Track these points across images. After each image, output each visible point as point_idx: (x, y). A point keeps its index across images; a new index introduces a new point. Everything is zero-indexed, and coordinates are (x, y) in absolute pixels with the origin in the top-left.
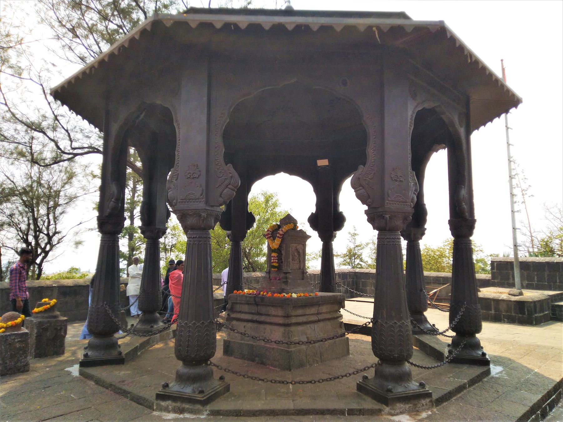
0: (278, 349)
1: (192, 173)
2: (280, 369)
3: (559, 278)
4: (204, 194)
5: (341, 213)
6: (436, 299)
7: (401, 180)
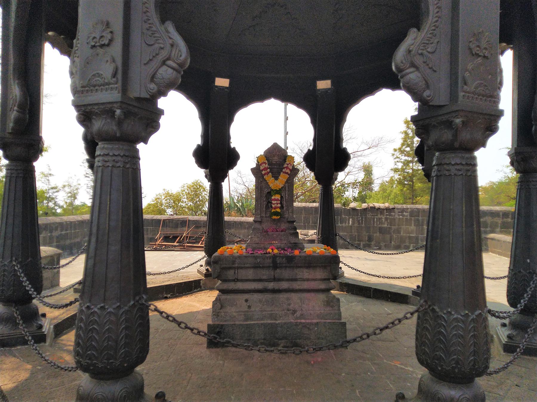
0: (325, 323)
1: (98, 37)
4: (120, 76)
7: (486, 55)
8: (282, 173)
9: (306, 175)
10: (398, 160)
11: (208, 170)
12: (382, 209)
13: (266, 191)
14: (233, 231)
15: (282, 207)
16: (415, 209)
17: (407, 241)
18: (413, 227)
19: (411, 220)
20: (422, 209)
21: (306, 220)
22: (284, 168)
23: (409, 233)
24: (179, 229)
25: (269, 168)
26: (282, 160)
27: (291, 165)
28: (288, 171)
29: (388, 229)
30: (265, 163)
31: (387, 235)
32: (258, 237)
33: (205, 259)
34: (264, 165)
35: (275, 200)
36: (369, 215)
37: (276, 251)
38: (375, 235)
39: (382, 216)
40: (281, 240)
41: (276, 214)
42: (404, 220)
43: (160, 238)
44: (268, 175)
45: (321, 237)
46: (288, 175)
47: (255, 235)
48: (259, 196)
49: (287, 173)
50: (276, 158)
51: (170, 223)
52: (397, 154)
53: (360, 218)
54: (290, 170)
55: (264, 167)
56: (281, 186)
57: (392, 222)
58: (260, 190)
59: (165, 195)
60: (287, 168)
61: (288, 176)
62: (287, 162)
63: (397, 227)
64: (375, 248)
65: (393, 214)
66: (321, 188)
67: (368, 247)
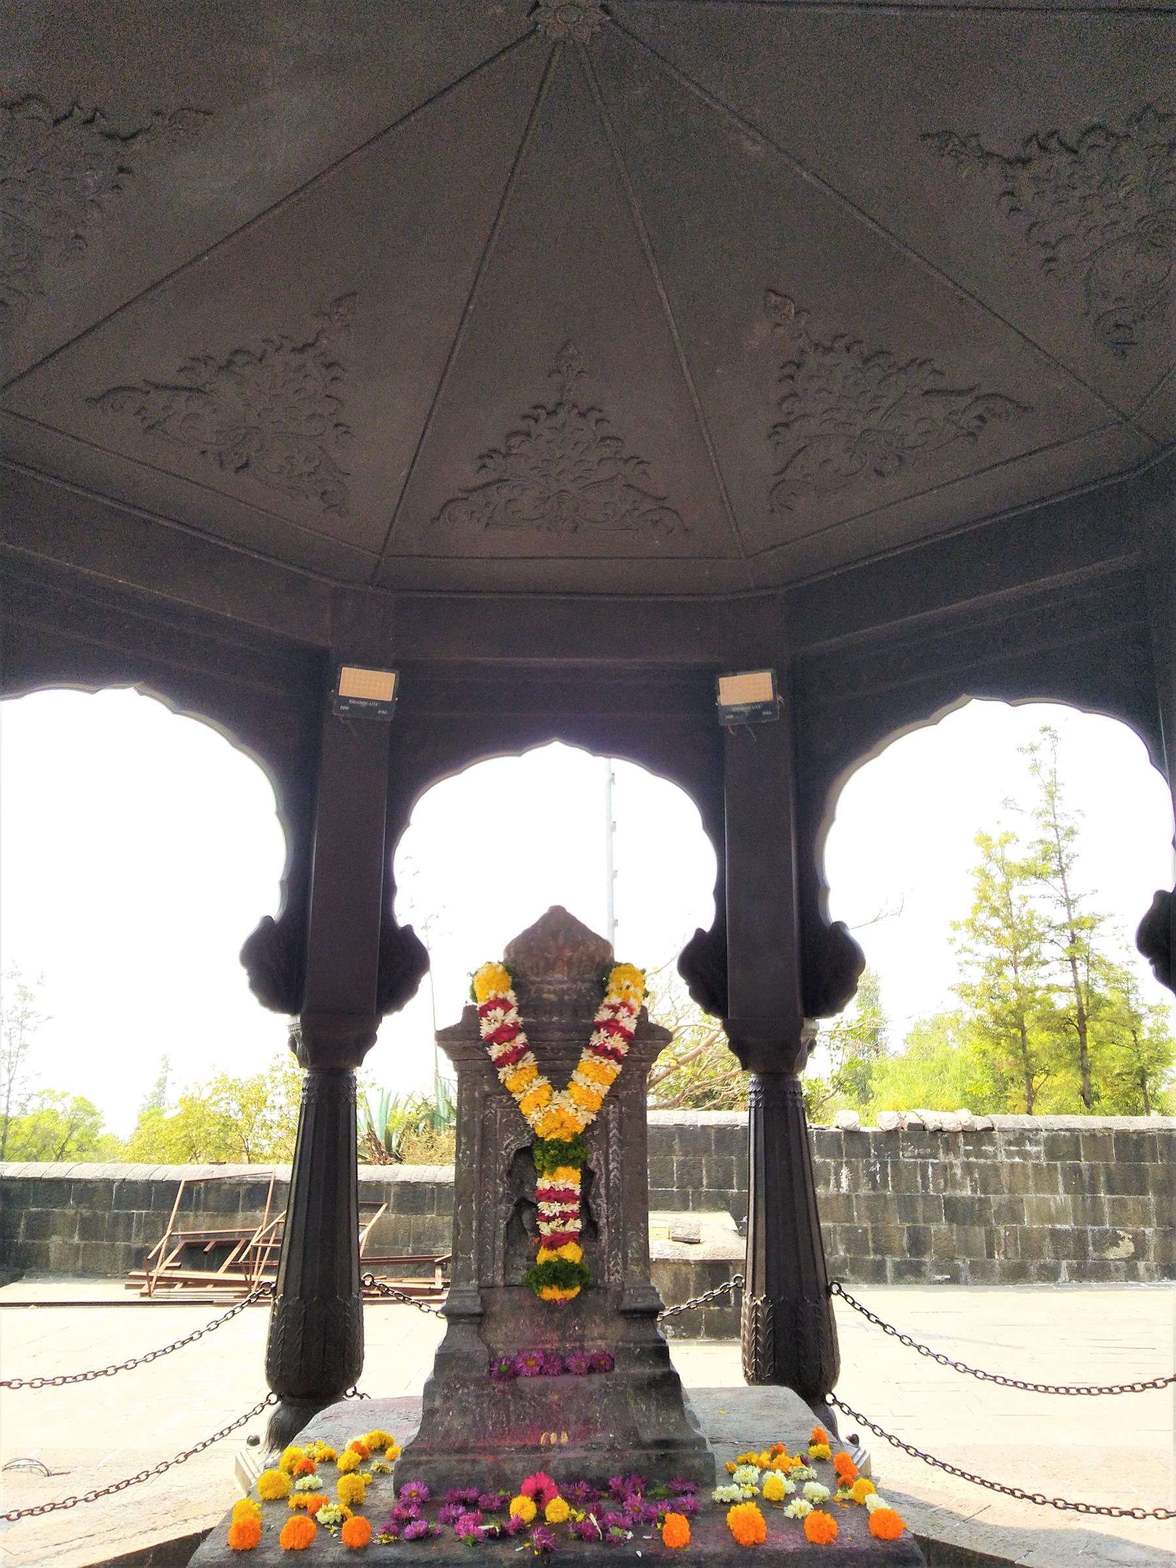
2: (821, 1511)
3: (707, 1172)
5: (839, 927)
6: (265, 1267)
8: (586, 1054)
9: (679, 1008)
10: (968, 957)
11: (298, 1019)
12: (948, 1132)
13: (511, 1143)
14: (432, 1219)
15: (591, 1231)
16: (1061, 1129)
17: (1047, 1246)
18: (1061, 1198)
19: (1052, 1169)
20: (1086, 1131)
21: (689, 1173)
22: (597, 1027)
23: (1051, 1219)
24: (240, 1216)
25: (526, 1028)
26: (587, 985)
27: (631, 1011)
28: (617, 1042)
29: (977, 1206)
30: (505, 1005)
31: (977, 1228)
32: (464, 1411)
33: (270, 1411)
34: (499, 1012)
35: (553, 1195)
36: (908, 1155)
37: (557, 1510)
38: (933, 1228)
39: (951, 1157)
40: (587, 1421)
41: (560, 1274)
42: (1030, 1172)
43: (169, 1251)
44: (520, 1065)
45: (764, 1301)
46: (619, 1062)
47: (446, 1398)
48: (475, 1176)
49: (613, 1054)
50: (558, 976)
51: (211, 1197)
52: (964, 937)
53: (875, 1164)
54: (627, 1037)
55: (497, 1025)
56: (584, 1118)
57: (988, 1179)
58: (477, 1140)
59: (214, 1085)
60: (612, 1026)
61: (619, 1068)
62: (614, 999)
63: (1006, 1196)
64: (939, 1277)
65: (990, 1149)
66: (754, 1083)
67: (911, 1274)
